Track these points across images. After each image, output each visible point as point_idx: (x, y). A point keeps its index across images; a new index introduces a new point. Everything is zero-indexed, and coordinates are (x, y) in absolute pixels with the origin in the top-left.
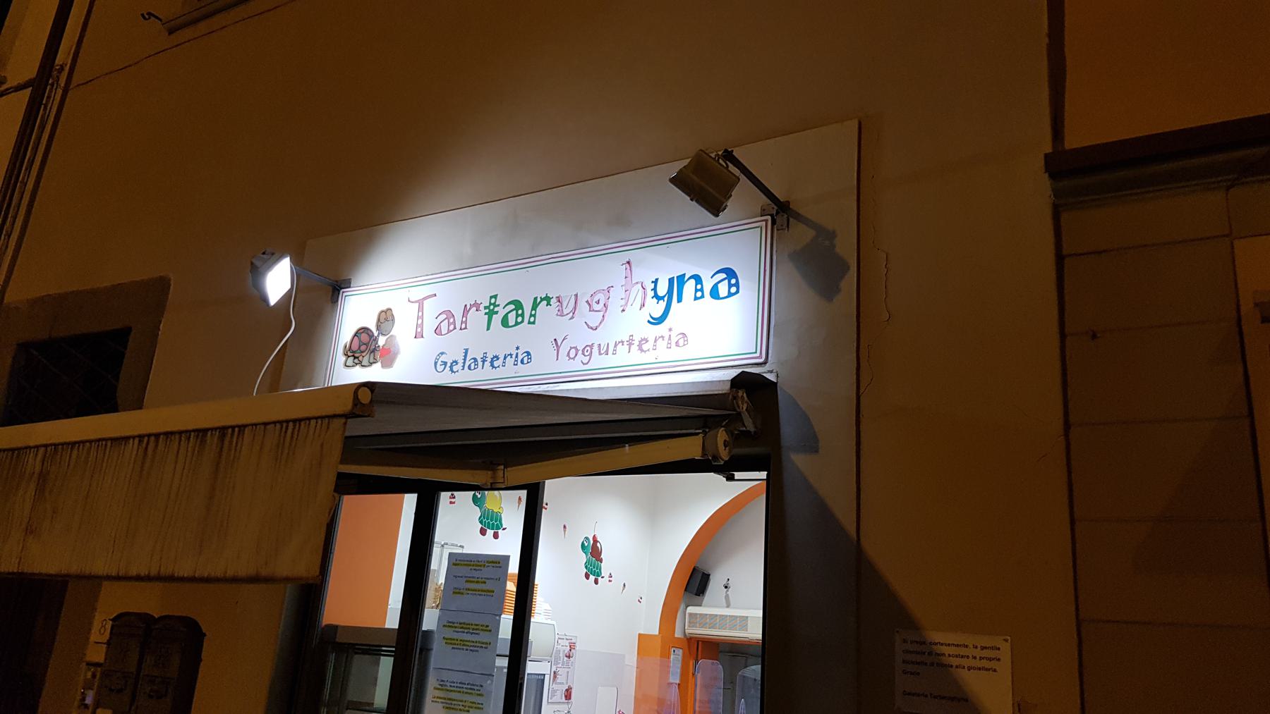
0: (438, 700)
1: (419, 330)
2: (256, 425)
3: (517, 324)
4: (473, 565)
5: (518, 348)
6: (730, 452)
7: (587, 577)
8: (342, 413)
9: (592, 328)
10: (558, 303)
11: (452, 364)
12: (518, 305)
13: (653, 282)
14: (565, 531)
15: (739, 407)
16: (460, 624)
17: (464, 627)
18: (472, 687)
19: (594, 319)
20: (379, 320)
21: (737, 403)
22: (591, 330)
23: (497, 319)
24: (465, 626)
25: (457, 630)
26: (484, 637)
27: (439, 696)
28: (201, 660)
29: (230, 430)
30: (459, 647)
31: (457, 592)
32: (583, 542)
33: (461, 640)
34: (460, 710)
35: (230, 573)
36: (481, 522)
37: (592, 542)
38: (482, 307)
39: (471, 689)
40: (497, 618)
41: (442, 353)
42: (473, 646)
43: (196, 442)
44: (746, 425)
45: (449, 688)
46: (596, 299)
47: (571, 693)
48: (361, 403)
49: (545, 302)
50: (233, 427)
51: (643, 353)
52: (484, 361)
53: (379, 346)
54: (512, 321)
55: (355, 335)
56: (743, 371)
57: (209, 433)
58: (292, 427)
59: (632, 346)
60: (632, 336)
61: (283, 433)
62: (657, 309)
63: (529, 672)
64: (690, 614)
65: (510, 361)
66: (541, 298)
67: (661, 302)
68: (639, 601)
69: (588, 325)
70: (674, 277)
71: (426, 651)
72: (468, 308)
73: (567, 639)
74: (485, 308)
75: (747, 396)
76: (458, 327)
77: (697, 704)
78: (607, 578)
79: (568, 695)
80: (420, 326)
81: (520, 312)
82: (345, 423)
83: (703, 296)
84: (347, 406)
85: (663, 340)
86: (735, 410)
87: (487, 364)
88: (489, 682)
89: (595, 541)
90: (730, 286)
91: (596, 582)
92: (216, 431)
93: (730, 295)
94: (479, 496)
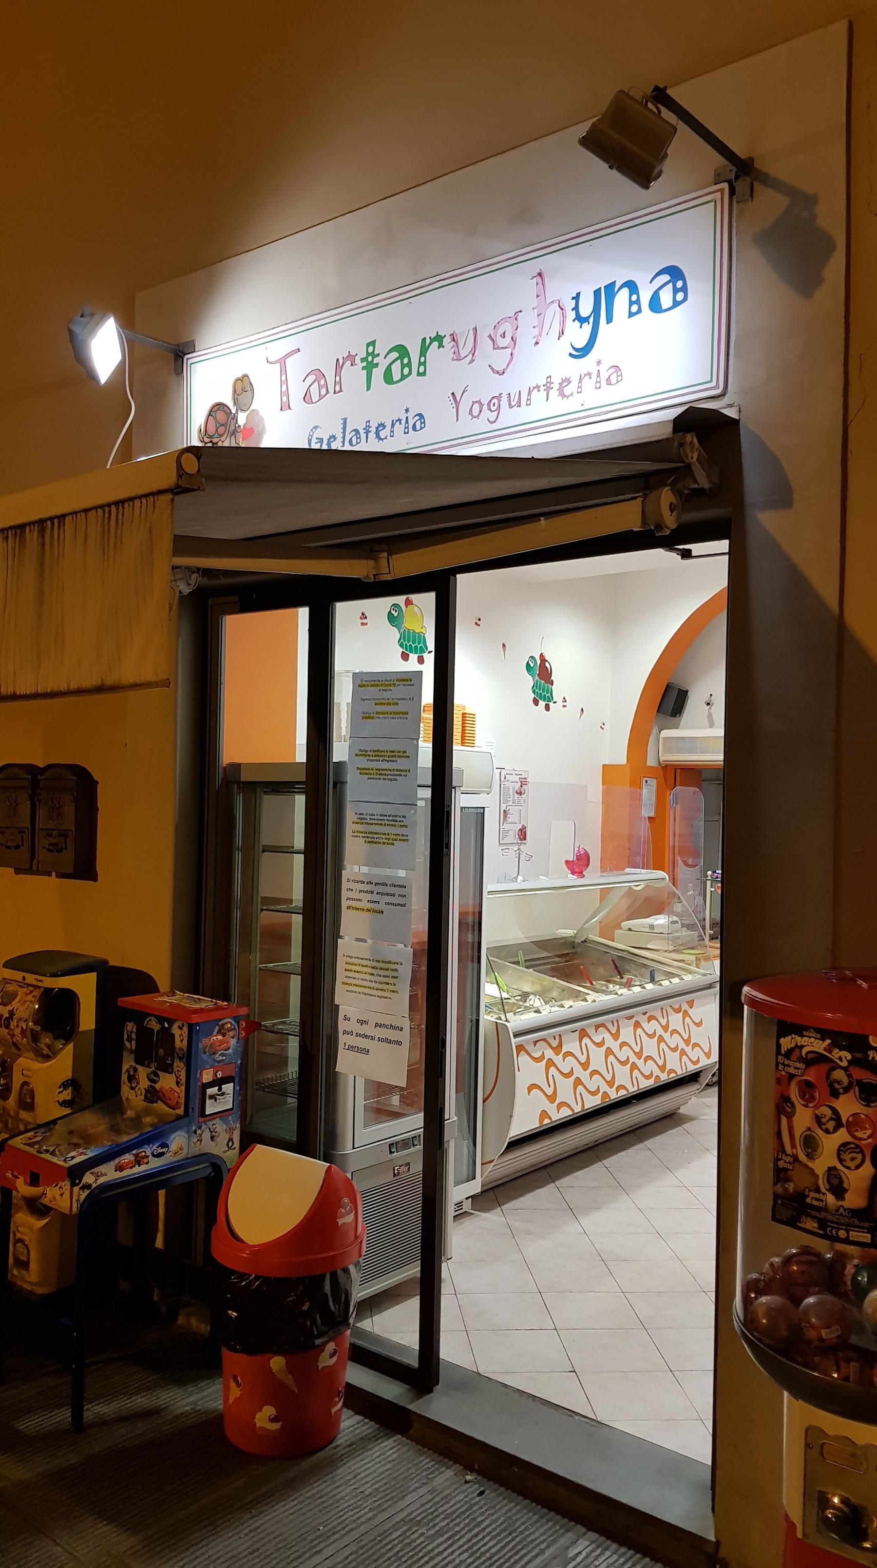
0: (358, 834)
1: (285, 399)
2: (76, 513)
3: (403, 377)
4: (382, 685)
5: (407, 411)
6: (678, 519)
7: (536, 702)
8: (167, 487)
9: (498, 373)
10: (453, 343)
11: (329, 440)
12: (402, 351)
13: (573, 298)
14: (504, 651)
15: (687, 456)
16: (374, 751)
17: (378, 754)
18: (395, 818)
19: (500, 359)
20: (235, 391)
21: (685, 452)
22: (497, 375)
23: (378, 374)
24: (379, 753)
25: (371, 758)
26: (401, 764)
27: (359, 830)
28: (98, 810)
29: (49, 523)
30: (375, 776)
31: (367, 716)
32: (528, 662)
33: (376, 770)
34: (384, 843)
35: (74, 686)
36: (401, 645)
37: (539, 662)
38: (358, 360)
39: (393, 820)
40: (415, 742)
41: (316, 427)
42: (391, 775)
43: (15, 538)
44: (699, 481)
45: (369, 821)
46: (500, 332)
47: (525, 832)
48: (187, 473)
49: (436, 344)
50: (51, 519)
51: (565, 399)
52: (367, 432)
53: (239, 426)
54: (396, 375)
55: (209, 415)
56: (690, 407)
57: (27, 529)
58: (116, 512)
59: (551, 391)
60: (550, 377)
61: (106, 521)
62: (579, 335)
63: (462, 805)
64: (666, 739)
65: (399, 428)
66: (430, 338)
67: (585, 325)
68: (601, 727)
69: (493, 369)
70: (600, 288)
71: (339, 783)
72: (341, 364)
73: (516, 774)
74: (362, 360)
75: (699, 443)
76: (331, 390)
77: (677, 839)
78: (560, 703)
79: (523, 834)
80: (285, 393)
81: (406, 361)
82: (173, 500)
83: (639, 311)
84: (169, 479)
85: (590, 378)
86: (682, 462)
87: (372, 435)
88: (412, 812)
89: (543, 659)
90: (676, 291)
91: (547, 708)
92: (34, 526)
93: (676, 304)
94: (396, 614)
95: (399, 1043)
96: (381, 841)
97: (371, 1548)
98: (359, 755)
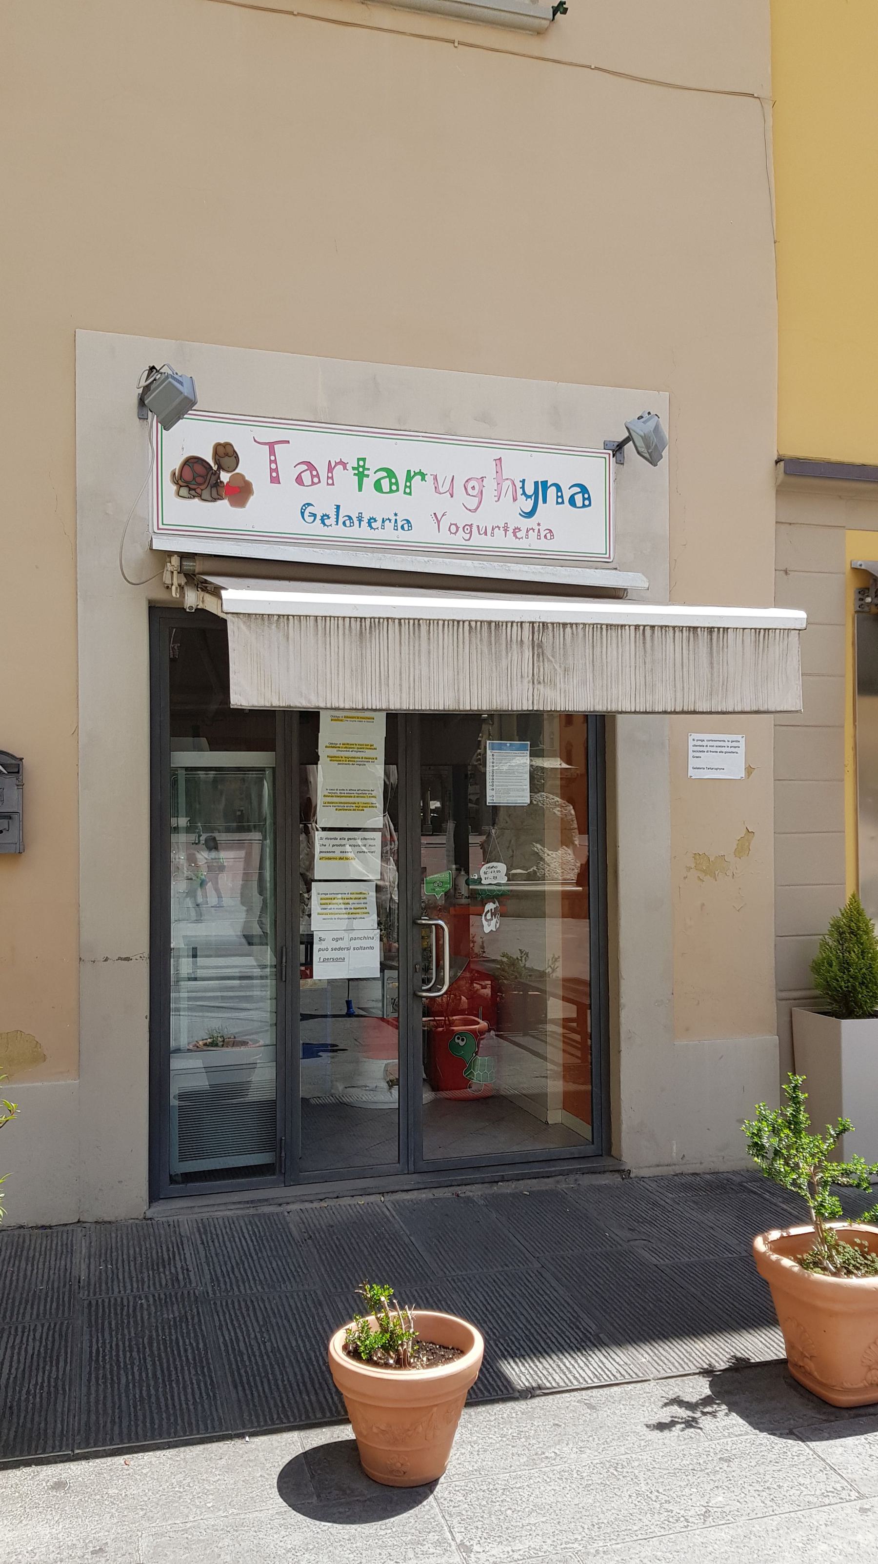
23: (368, 483)
53: (222, 482)
62: (528, 505)
95: (372, 948)
96: (352, 808)
97: (710, 1356)
98: (329, 747)
